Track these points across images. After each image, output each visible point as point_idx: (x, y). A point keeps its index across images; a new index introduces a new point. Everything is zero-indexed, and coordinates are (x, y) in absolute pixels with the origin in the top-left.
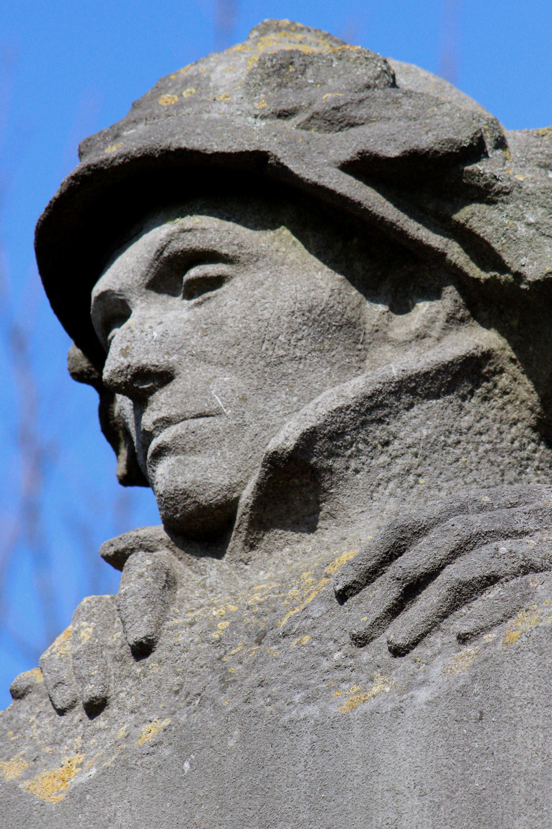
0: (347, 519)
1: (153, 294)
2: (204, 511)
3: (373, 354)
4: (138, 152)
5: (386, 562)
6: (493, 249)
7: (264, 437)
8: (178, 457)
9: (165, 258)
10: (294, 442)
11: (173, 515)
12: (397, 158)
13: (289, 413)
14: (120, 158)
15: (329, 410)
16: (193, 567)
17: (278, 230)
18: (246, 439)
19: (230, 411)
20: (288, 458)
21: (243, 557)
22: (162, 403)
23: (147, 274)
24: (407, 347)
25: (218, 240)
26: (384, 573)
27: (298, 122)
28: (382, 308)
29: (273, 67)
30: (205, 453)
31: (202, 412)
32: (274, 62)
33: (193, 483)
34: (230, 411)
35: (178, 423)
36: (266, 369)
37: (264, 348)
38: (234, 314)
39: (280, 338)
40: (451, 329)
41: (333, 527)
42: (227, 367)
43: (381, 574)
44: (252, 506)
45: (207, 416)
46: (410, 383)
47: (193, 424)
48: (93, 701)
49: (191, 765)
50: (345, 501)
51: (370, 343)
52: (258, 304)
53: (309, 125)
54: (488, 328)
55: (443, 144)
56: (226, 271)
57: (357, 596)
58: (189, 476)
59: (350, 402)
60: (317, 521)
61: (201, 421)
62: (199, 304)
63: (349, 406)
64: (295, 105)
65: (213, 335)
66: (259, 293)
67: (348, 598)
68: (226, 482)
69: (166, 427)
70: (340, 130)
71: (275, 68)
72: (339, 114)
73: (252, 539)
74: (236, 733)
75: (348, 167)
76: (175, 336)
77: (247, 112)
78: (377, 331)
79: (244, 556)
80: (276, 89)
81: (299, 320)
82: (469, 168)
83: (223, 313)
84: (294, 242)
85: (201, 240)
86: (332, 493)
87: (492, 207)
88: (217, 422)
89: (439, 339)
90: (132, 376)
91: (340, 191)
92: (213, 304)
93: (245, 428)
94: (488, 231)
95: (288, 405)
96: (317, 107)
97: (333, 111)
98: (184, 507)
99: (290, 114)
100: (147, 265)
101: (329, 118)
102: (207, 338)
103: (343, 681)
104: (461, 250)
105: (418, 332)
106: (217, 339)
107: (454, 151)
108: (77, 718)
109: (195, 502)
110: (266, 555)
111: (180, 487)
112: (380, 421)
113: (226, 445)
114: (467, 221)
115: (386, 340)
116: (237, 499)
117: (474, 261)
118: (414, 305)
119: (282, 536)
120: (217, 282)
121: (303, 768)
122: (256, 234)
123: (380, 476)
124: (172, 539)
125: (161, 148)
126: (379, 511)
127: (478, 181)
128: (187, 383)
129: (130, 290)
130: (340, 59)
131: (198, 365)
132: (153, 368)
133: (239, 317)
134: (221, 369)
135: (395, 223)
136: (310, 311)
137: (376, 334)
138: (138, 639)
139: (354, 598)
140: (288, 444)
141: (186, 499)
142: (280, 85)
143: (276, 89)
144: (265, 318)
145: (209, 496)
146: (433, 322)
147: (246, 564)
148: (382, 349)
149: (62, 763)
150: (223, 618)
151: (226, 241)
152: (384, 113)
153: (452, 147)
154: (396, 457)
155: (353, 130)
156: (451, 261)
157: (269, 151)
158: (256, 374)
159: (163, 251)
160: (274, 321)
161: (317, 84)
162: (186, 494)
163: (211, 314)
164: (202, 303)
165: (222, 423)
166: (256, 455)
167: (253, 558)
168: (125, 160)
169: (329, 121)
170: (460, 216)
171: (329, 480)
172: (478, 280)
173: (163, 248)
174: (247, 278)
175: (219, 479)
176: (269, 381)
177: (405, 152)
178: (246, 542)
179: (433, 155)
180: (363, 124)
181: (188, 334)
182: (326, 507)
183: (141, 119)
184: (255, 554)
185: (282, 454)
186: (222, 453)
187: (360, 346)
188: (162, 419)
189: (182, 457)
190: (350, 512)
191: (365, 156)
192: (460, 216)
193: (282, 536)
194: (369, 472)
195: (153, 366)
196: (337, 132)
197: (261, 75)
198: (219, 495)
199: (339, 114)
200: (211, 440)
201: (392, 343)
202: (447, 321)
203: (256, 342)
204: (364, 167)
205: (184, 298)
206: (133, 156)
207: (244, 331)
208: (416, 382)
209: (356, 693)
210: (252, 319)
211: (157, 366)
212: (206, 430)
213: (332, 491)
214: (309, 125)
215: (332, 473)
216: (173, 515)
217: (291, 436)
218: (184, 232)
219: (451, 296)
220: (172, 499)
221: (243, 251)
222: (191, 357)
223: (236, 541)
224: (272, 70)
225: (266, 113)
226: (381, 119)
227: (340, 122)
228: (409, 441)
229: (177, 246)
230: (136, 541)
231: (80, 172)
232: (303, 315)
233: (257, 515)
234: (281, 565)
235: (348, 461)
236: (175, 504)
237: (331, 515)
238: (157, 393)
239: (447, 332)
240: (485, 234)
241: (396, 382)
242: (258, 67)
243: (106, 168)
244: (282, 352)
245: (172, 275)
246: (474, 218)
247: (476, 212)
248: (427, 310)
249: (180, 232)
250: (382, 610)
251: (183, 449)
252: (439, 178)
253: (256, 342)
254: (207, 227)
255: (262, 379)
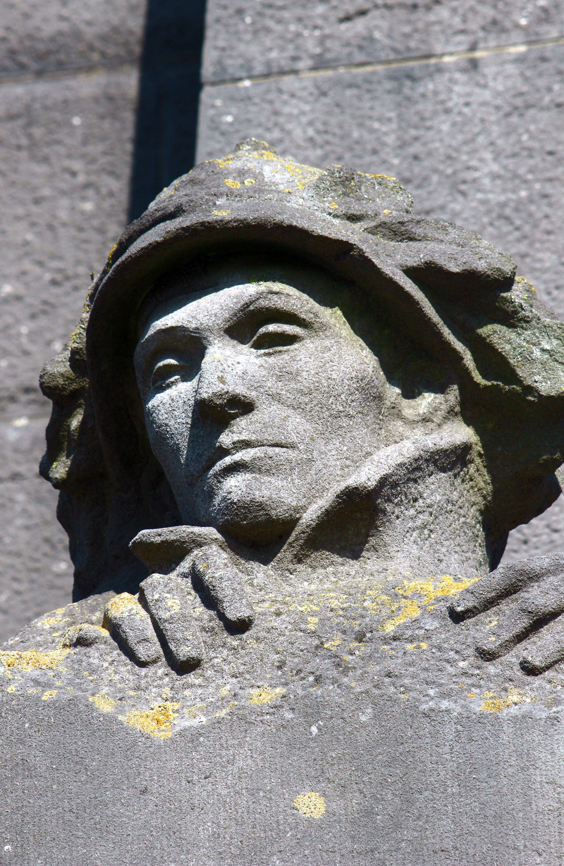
0: (387, 554)
1: (227, 338)
2: (271, 522)
3: (388, 425)
4: (253, 221)
5: (503, 596)
6: (509, 363)
7: (324, 474)
8: (254, 475)
9: (250, 310)
10: (374, 483)
11: (240, 522)
12: (457, 274)
13: (341, 459)
14: (235, 222)
15: (396, 463)
16: (241, 567)
17: (334, 309)
18: (313, 472)
19: (302, 447)
20: (366, 495)
21: (290, 567)
22: (241, 429)
23: (229, 321)
24: (415, 426)
25: (299, 306)
26: (498, 605)
27: (365, 227)
28: (398, 391)
29: (340, 178)
30: (278, 476)
31: (280, 442)
32: (341, 174)
33: (270, 498)
34: (302, 447)
35: (256, 447)
36: (329, 419)
37: (330, 402)
38: (308, 369)
39: (342, 396)
40: (449, 419)
41: (374, 559)
42: (297, 411)
43: (496, 605)
44: (313, 528)
45: (282, 447)
46: (436, 455)
47: (271, 451)
48: (190, 661)
49: (319, 729)
50: (387, 539)
51: (386, 416)
52: (327, 365)
53: (375, 231)
54: (468, 425)
55: (494, 271)
56: (300, 332)
57: (473, 619)
58: (266, 493)
59: (406, 461)
60: (362, 551)
61: (277, 450)
62: (269, 354)
63: (406, 464)
64: (362, 212)
65: (287, 382)
66: (328, 356)
67: (465, 619)
68: (294, 504)
69: (244, 448)
70: (401, 241)
71: (342, 179)
72: (403, 228)
73: (302, 554)
74: (369, 711)
75: (410, 272)
76: (254, 376)
77: (322, 209)
78: (394, 408)
79: (291, 566)
80: (342, 196)
81: (355, 386)
82: (502, 294)
83: (299, 366)
84: (344, 322)
85: (286, 304)
86: (380, 531)
87: (511, 330)
88: (291, 454)
89: (439, 425)
90: (227, 400)
91: (407, 289)
92: (286, 357)
93: (313, 463)
94: (506, 348)
95: (340, 452)
96: (382, 218)
97: (398, 225)
98: (255, 516)
99: (357, 219)
100: (231, 313)
101: (395, 230)
102: (281, 383)
103: (473, 685)
104: (472, 358)
105: (425, 416)
106: (292, 386)
107: (500, 278)
108: (160, 672)
109: (267, 514)
110: (310, 570)
111: (257, 500)
112: (415, 481)
113: (296, 473)
114: (488, 336)
115: (399, 416)
116: (299, 519)
117: (478, 370)
118: (420, 394)
119: (329, 557)
120: (291, 339)
121: (449, 751)
122: (322, 308)
123: (409, 525)
124: (226, 541)
125: (275, 222)
126: (408, 553)
127: (508, 307)
128: (265, 416)
129: (210, 330)
130: (380, 184)
131: (273, 403)
132: (242, 398)
133: (313, 372)
134: (292, 411)
135: (429, 326)
136: (362, 380)
137: (392, 410)
138: (243, 617)
139: (470, 620)
140: (370, 484)
141: (260, 510)
142: (344, 194)
143: (342, 196)
144: (333, 377)
145: (279, 512)
146: (436, 411)
147: (291, 574)
148: (395, 423)
149: (152, 706)
150: (314, 614)
151: (305, 308)
152: (437, 236)
153: (499, 275)
154: (420, 512)
155: (411, 243)
156: (465, 365)
157: (355, 245)
158: (322, 421)
159: (250, 305)
160: (339, 381)
161: (370, 200)
162: (261, 506)
163: (286, 365)
164: (273, 354)
165: (295, 455)
166: (318, 487)
167: (298, 570)
168: (239, 224)
169: (394, 231)
170: (485, 331)
171: (381, 519)
172: (479, 384)
173: (251, 303)
174: (317, 342)
175: (289, 500)
176: (330, 429)
177: (465, 270)
178: (296, 556)
179: (484, 278)
180: (420, 240)
181: (264, 377)
182: (372, 541)
183: (222, 194)
184: (300, 567)
185: (362, 490)
186: (292, 480)
187: (381, 417)
188: (243, 441)
189: (258, 476)
190: (390, 549)
191: (431, 266)
192: (485, 331)
193: (329, 557)
194: (403, 520)
195: (244, 396)
196: (398, 242)
197: (330, 181)
198: (287, 512)
199: (403, 228)
200: (285, 467)
201: (404, 420)
202: (448, 413)
203: (325, 395)
204: (427, 275)
205: (252, 347)
206: (248, 223)
207: (317, 384)
208: (440, 456)
209: (492, 698)
210: (323, 376)
211: (246, 397)
212: (282, 458)
213: (380, 529)
214: (375, 231)
215: (385, 514)
216: (240, 522)
217: (373, 477)
218: (272, 293)
219: (453, 394)
220: (244, 508)
221: (317, 320)
222: (267, 396)
223: (285, 554)
224: (339, 180)
225: (340, 213)
226: (435, 240)
227: (403, 235)
228: (429, 501)
229: (263, 303)
230: (191, 536)
231: (193, 226)
232: (358, 382)
233: (314, 535)
234: (325, 580)
235: (394, 508)
236: (246, 513)
237: (375, 549)
238: (238, 419)
239: (446, 421)
240: (504, 350)
241: (431, 453)
242: (328, 175)
243: (218, 227)
244: (341, 408)
245: (246, 326)
246: (495, 335)
247: (498, 330)
248: (432, 400)
249: (268, 293)
250: (511, 635)
251: (260, 470)
252: (478, 296)
253: (325, 395)
254: (291, 294)
255: (325, 427)
